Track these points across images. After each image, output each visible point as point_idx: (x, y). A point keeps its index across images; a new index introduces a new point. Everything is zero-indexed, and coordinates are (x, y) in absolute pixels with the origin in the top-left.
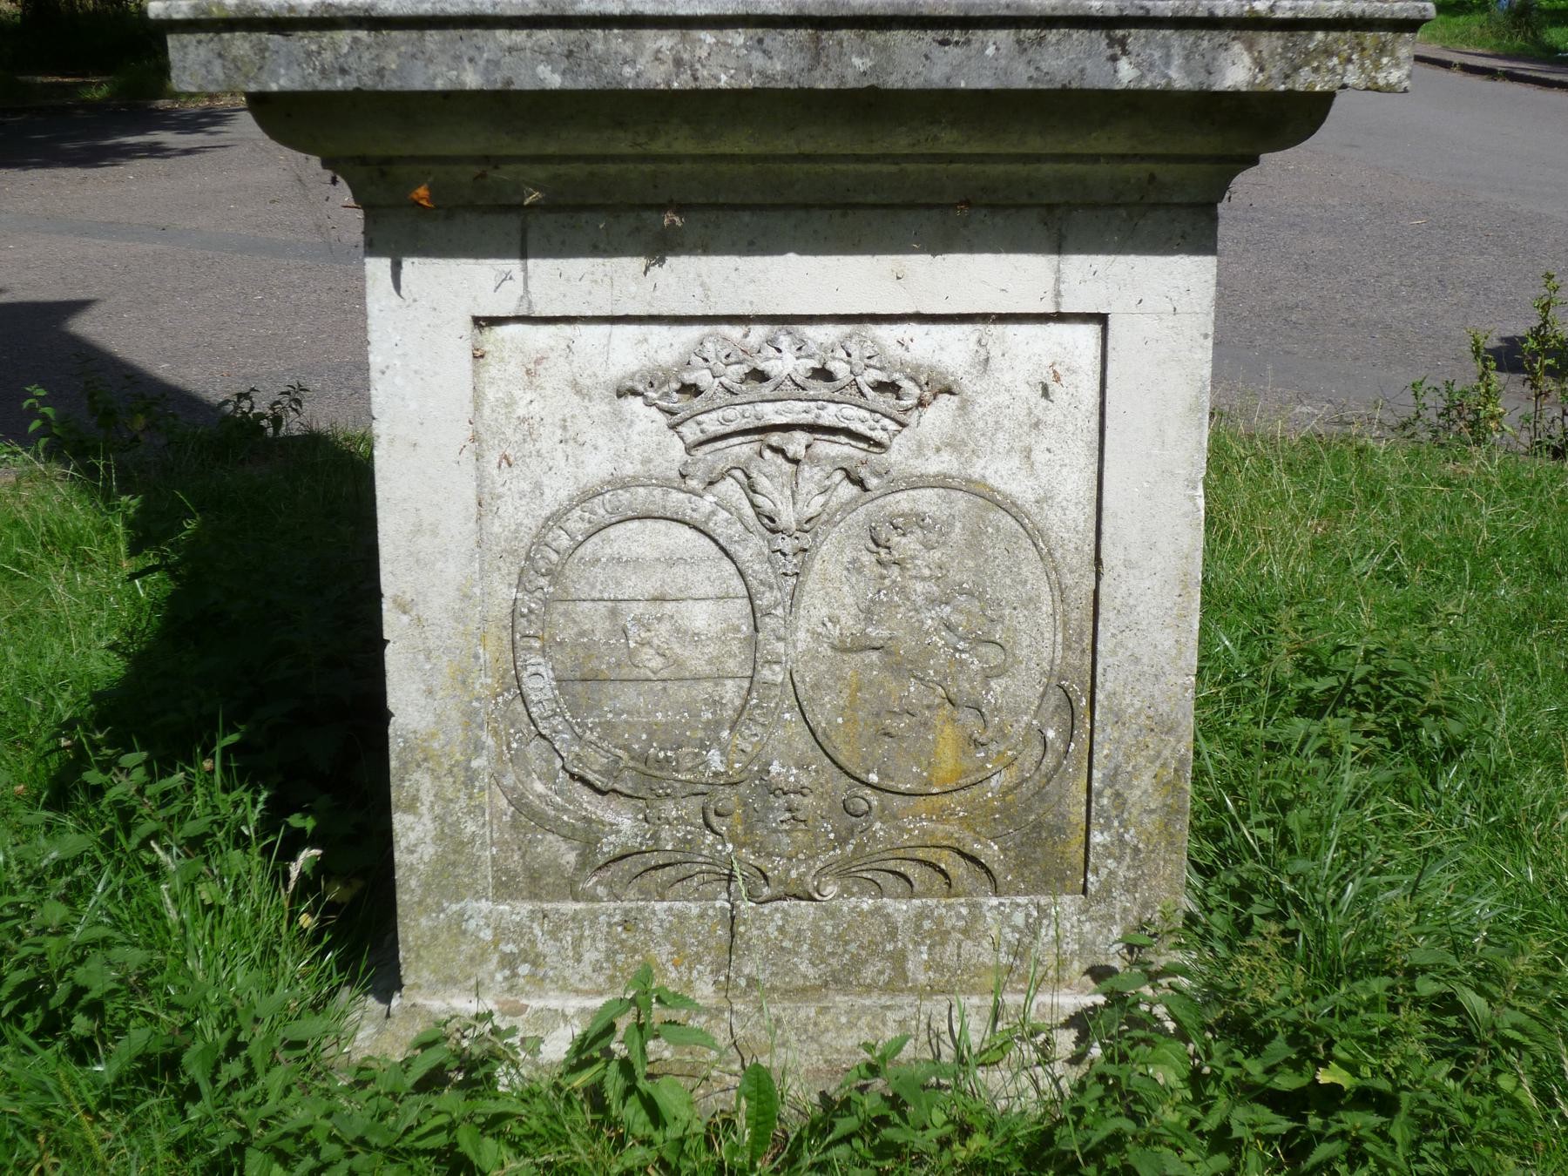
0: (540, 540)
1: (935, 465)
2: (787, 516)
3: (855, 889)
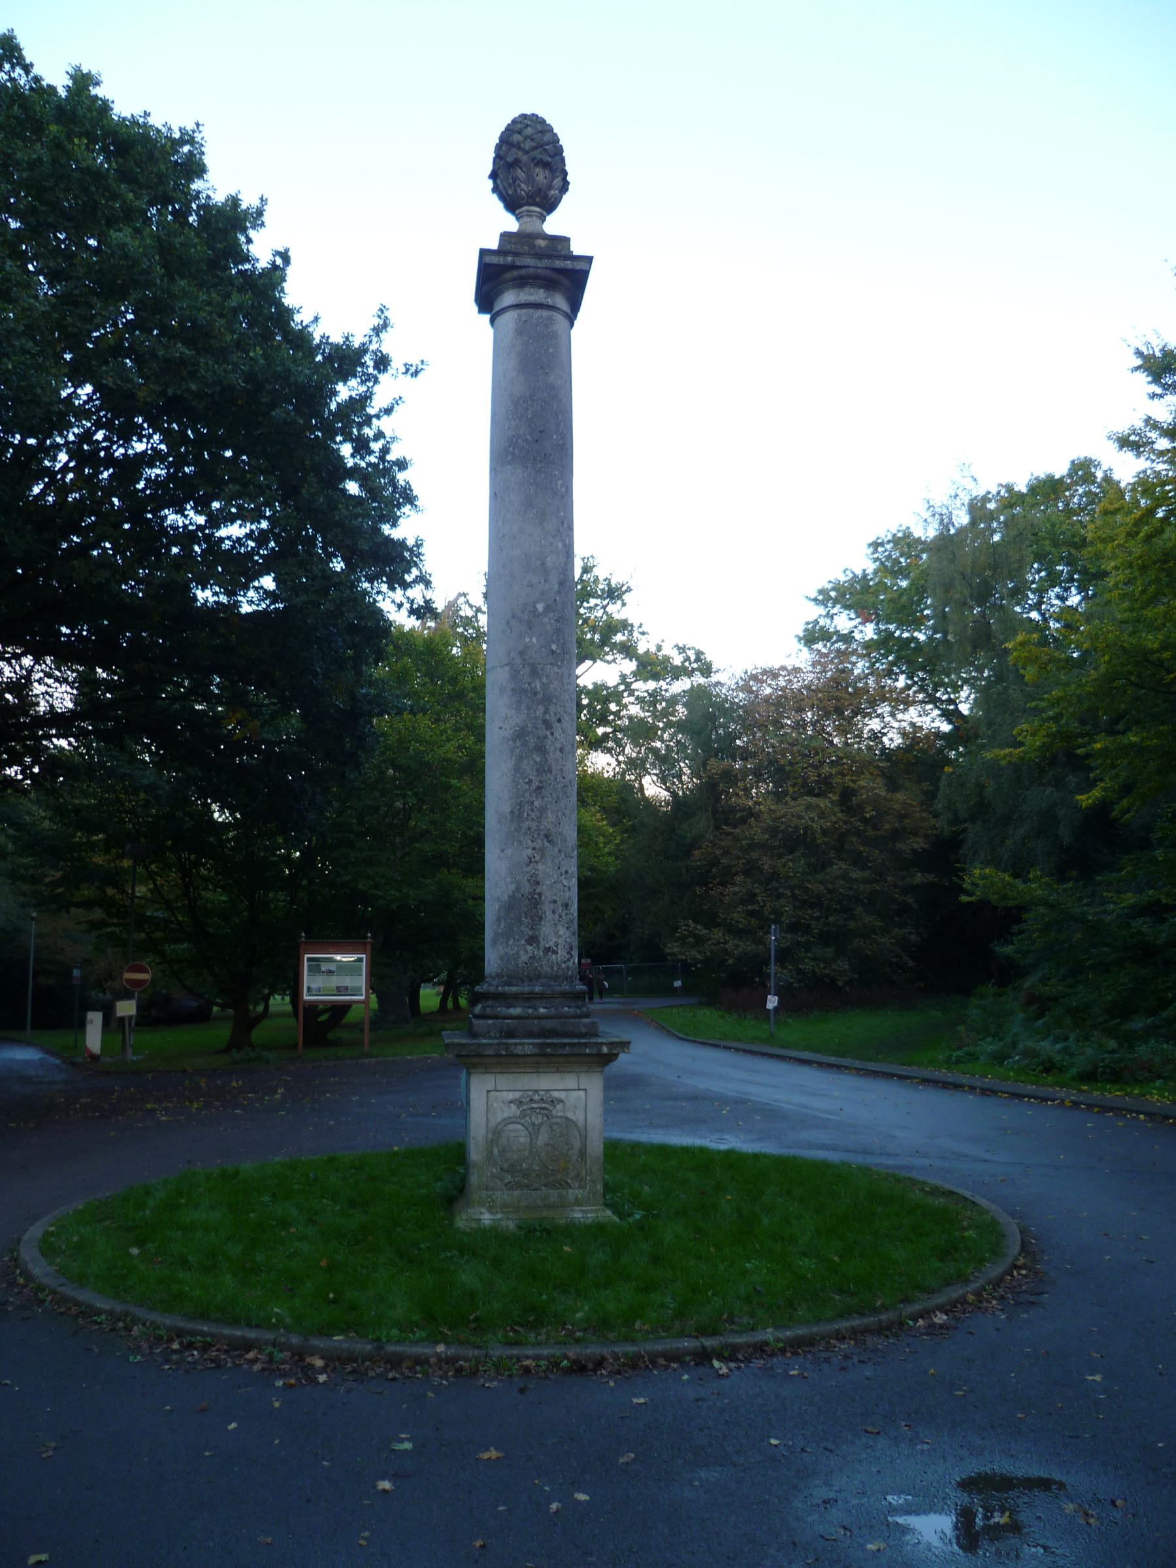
0: (497, 1126)
1: (560, 1114)
2: (537, 1123)
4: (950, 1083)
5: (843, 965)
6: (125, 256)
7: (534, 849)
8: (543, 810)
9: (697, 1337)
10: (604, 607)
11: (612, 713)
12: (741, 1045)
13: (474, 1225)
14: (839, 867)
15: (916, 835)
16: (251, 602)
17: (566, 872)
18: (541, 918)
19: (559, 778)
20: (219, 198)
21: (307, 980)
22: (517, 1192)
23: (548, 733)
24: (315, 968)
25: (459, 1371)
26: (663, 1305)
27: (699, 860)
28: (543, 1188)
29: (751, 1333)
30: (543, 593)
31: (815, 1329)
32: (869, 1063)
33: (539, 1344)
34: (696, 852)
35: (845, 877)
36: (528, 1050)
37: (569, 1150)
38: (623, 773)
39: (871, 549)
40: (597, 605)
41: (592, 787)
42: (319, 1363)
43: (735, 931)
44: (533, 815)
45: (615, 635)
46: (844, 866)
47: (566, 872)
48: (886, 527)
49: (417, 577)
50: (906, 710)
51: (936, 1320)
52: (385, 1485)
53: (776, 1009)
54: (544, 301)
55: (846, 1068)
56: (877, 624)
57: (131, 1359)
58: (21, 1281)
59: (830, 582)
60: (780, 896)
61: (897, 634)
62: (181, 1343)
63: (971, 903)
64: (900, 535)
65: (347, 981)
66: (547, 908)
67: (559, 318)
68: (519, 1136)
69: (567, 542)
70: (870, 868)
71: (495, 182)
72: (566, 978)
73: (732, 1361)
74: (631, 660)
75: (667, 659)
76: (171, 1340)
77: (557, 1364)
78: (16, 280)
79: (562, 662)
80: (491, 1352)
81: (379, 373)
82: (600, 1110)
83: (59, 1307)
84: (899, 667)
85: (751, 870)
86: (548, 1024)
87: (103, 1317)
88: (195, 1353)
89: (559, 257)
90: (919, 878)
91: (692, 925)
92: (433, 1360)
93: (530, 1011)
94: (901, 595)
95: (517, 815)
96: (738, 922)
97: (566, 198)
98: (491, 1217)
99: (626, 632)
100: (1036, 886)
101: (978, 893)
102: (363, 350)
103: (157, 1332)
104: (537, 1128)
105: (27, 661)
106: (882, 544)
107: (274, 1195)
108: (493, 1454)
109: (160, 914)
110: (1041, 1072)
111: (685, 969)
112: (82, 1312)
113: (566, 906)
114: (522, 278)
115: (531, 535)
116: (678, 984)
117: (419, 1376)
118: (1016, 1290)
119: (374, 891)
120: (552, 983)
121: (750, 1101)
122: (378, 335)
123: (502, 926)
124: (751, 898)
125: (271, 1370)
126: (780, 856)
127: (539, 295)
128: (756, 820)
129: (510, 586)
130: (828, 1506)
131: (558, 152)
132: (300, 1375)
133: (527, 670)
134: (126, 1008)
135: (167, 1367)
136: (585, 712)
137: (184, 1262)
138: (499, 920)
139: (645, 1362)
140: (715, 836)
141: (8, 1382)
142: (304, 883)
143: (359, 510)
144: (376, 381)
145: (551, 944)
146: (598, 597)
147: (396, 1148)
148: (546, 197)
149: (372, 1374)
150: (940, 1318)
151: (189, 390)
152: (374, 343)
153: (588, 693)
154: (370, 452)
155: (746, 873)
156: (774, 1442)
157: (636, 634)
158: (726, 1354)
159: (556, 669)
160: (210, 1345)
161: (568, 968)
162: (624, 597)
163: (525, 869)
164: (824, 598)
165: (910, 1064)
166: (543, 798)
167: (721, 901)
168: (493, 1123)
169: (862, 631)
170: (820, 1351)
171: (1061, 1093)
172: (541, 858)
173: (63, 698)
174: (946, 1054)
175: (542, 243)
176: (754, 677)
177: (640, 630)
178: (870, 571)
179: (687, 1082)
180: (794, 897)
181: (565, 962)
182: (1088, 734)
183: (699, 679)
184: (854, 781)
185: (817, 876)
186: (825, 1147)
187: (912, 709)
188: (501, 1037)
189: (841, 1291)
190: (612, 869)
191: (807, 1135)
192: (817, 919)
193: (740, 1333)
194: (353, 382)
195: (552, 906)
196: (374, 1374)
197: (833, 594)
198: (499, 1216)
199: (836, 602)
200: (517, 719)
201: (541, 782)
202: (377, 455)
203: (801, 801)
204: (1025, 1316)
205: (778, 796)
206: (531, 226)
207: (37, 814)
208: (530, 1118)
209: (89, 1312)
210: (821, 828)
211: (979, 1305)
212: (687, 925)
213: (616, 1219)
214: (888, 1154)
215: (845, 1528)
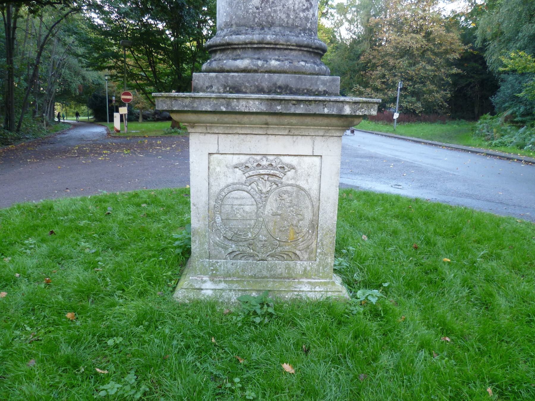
0: (219, 194)
1: (290, 182)
2: (264, 190)
5: (419, 105)
27: (363, 61)
28: (270, 259)
36: (254, 106)
37: (299, 221)
60: (395, 76)
70: (434, 65)
72: (304, 30)
86: (281, 79)
90: (455, 71)
93: (260, 63)
98: (213, 287)
104: (264, 196)
124: (384, 76)
126: (397, 59)
155: (382, 66)
168: (215, 189)
179: (364, 148)
192: (410, 86)
198: (222, 285)
208: (258, 185)
210: (416, 47)
212: (356, 87)
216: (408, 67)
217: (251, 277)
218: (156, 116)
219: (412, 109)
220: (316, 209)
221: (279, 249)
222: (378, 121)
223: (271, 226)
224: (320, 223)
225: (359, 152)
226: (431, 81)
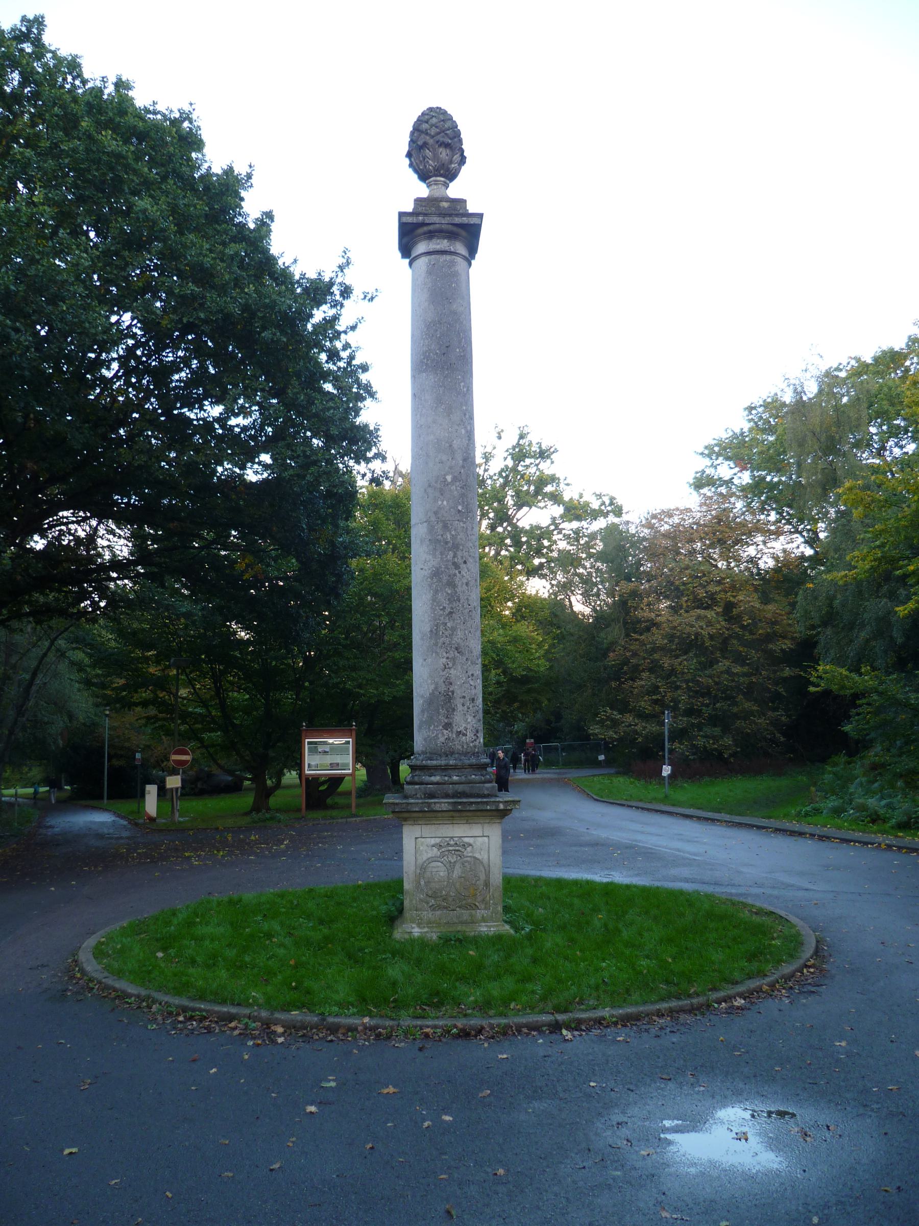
0: (423, 865)
1: (469, 855)
2: (452, 861)
3: (695, 527)
4: (795, 832)
5: (728, 741)
6: (147, 219)
7: (448, 658)
8: (453, 629)
9: (553, 1014)
10: (537, 465)
11: (545, 547)
12: (641, 804)
13: (407, 936)
14: (724, 664)
15: (784, 637)
16: (256, 473)
17: (472, 675)
18: (454, 710)
19: (466, 605)
20: (217, 170)
21: (308, 759)
22: (438, 913)
23: (457, 572)
24: (314, 750)
25: (378, 1036)
26: (533, 992)
28: (458, 909)
29: (594, 1011)
30: (451, 468)
31: (641, 1009)
32: (737, 817)
33: (437, 1018)
34: (611, 654)
35: (728, 671)
36: (445, 807)
38: (556, 594)
39: (747, 412)
40: (531, 464)
41: (529, 605)
42: (280, 1030)
43: (642, 716)
44: (447, 633)
45: (546, 486)
46: (728, 664)
47: (472, 675)
48: (759, 394)
49: (375, 454)
50: (777, 538)
51: (736, 1004)
52: (312, 1109)
53: (669, 776)
54: (447, 249)
55: (718, 820)
56: (752, 472)
57: (149, 1027)
58: (78, 975)
59: (714, 439)
60: (678, 688)
61: (768, 478)
62: (185, 1017)
63: (818, 692)
64: (769, 400)
65: (338, 759)
66: (458, 702)
67: (459, 260)
68: (439, 871)
69: (469, 428)
70: (748, 665)
71: (410, 160)
73: (577, 1030)
74: (559, 506)
75: (587, 504)
76: (178, 1014)
77: (449, 1032)
78: (67, 243)
79: (466, 518)
80: (402, 1023)
81: (344, 299)
82: (499, 852)
83: (103, 993)
84: (769, 505)
85: (654, 668)
86: (460, 788)
87: (133, 999)
88: (194, 1023)
89: (457, 215)
90: (787, 672)
91: (609, 711)
92: (360, 1028)
93: (446, 778)
94: (769, 449)
95: (434, 633)
96: (644, 708)
97: (464, 169)
99: (554, 484)
100: (866, 680)
101: (823, 685)
102: (331, 284)
103: (169, 1009)
104: (452, 866)
105: (94, 523)
106: (755, 408)
107: (265, 916)
108: (391, 1089)
109: (198, 710)
110: (869, 822)
111: (605, 746)
112: (118, 996)
113: (473, 700)
114: (430, 232)
115: (441, 425)
116: (602, 757)
117: (350, 1039)
118: (802, 983)
119: (357, 690)
120: (463, 758)
121: (637, 846)
122: (342, 271)
123: (425, 716)
124: (655, 689)
125: (246, 1034)
126: (677, 657)
127: (444, 244)
128: (657, 628)
129: (427, 463)
130: (620, 1126)
131: (456, 135)
132: (266, 1038)
133: (440, 525)
134: (174, 782)
135: (173, 1032)
136: (525, 547)
137: (193, 962)
138: (423, 711)
139: (512, 1031)
140: (626, 641)
141: (63, 1041)
142: (307, 684)
143: (331, 404)
144: (342, 306)
145: (462, 728)
146: (532, 457)
147: (360, 882)
148: (448, 170)
149: (316, 1037)
150: (740, 1002)
151: (198, 318)
152: (339, 276)
153: (526, 532)
154: (340, 359)
155: (651, 670)
156: (592, 1084)
157: (562, 486)
158: (573, 1026)
159: (462, 524)
160: (205, 1018)
161: (475, 746)
162: (552, 457)
163: (441, 673)
164: (710, 452)
165: (769, 818)
166: (454, 620)
167: (631, 692)
168: (420, 862)
169: (740, 478)
170: (643, 1024)
171: (880, 838)
172: (453, 665)
173: (123, 548)
174: (798, 809)
175: (445, 205)
176: (654, 516)
177: (566, 482)
178: (746, 430)
180: (689, 688)
181: (473, 742)
182: (908, 558)
183: (612, 519)
184: (734, 597)
185: (706, 672)
186: (687, 880)
187: (782, 538)
188: (425, 798)
189: (667, 982)
190: (542, 669)
191: (674, 872)
192: (707, 706)
193: (586, 1011)
194: (324, 307)
195: (462, 700)
196: (317, 1037)
197: (716, 449)
198: (426, 930)
199: (718, 455)
200: (434, 562)
201: (452, 608)
202: (345, 361)
203: (693, 613)
204: (804, 1001)
205: (674, 609)
206: (438, 192)
207: (108, 637)
209: (123, 996)
210: (709, 634)
211: (772, 993)
212: (605, 711)
213: (512, 932)
214: (733, 885)
215: (628, 1140)
216: (699, 670)
217: (446, 923)
218: (199, 785)
219: (716, 749)
220: (487, 871)
221: (464, 902)
222: (651, 778)
223: (458, 885)
224: (491, 881)
225: (582, 838)
226: (744, 694)
